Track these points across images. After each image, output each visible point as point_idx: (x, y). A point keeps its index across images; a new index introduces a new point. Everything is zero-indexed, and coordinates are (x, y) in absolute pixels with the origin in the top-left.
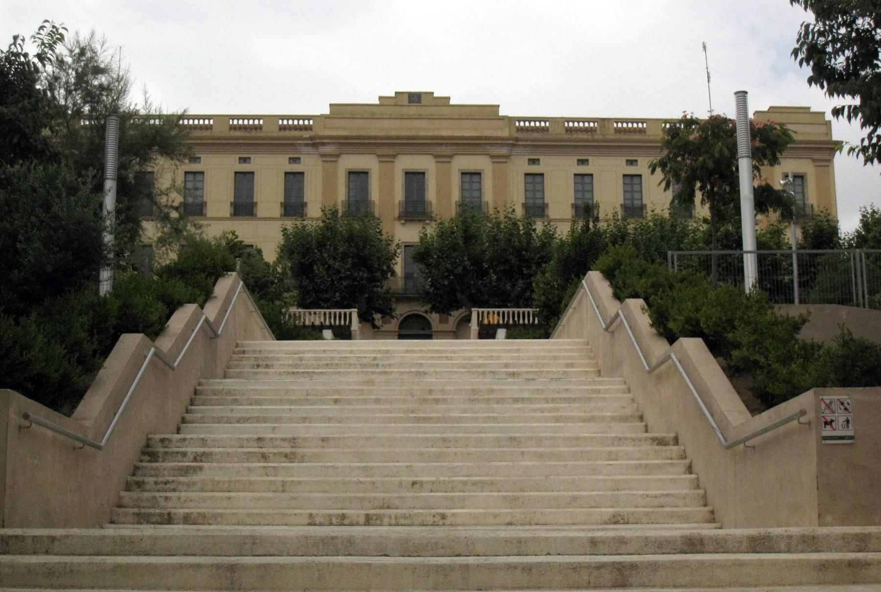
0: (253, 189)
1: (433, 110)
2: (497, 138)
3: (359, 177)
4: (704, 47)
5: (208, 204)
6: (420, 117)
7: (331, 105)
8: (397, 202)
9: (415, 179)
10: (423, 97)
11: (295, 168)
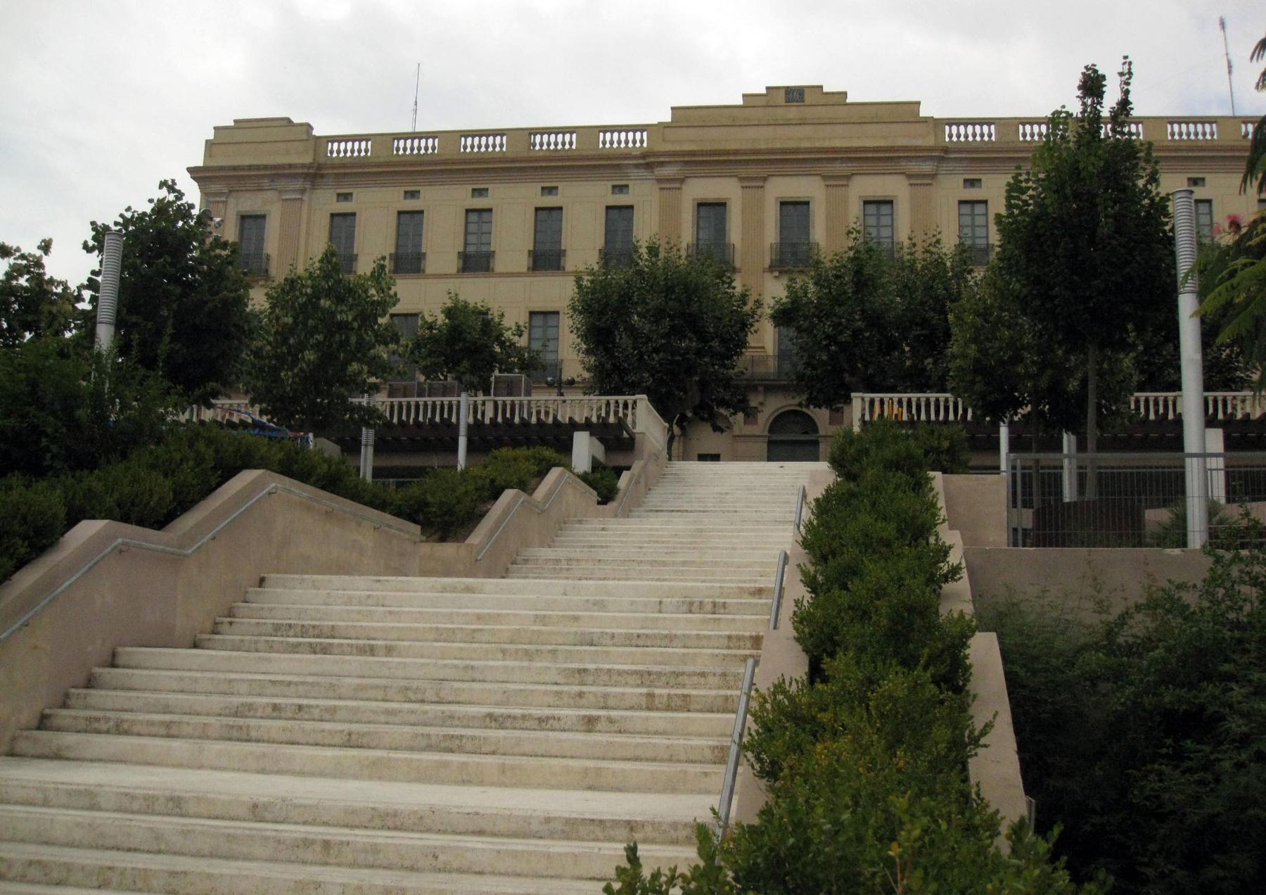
0: (560, 231)
1: (821, 112)
2: (916, 149)
3: (713, 210)
4: (1223, 24)
5: (569, 253)
6: (802, 123)
7: (673, 109)
8: (767, 246)
9: (795, 210)
10: (807, 92)
11: (621, 199)
